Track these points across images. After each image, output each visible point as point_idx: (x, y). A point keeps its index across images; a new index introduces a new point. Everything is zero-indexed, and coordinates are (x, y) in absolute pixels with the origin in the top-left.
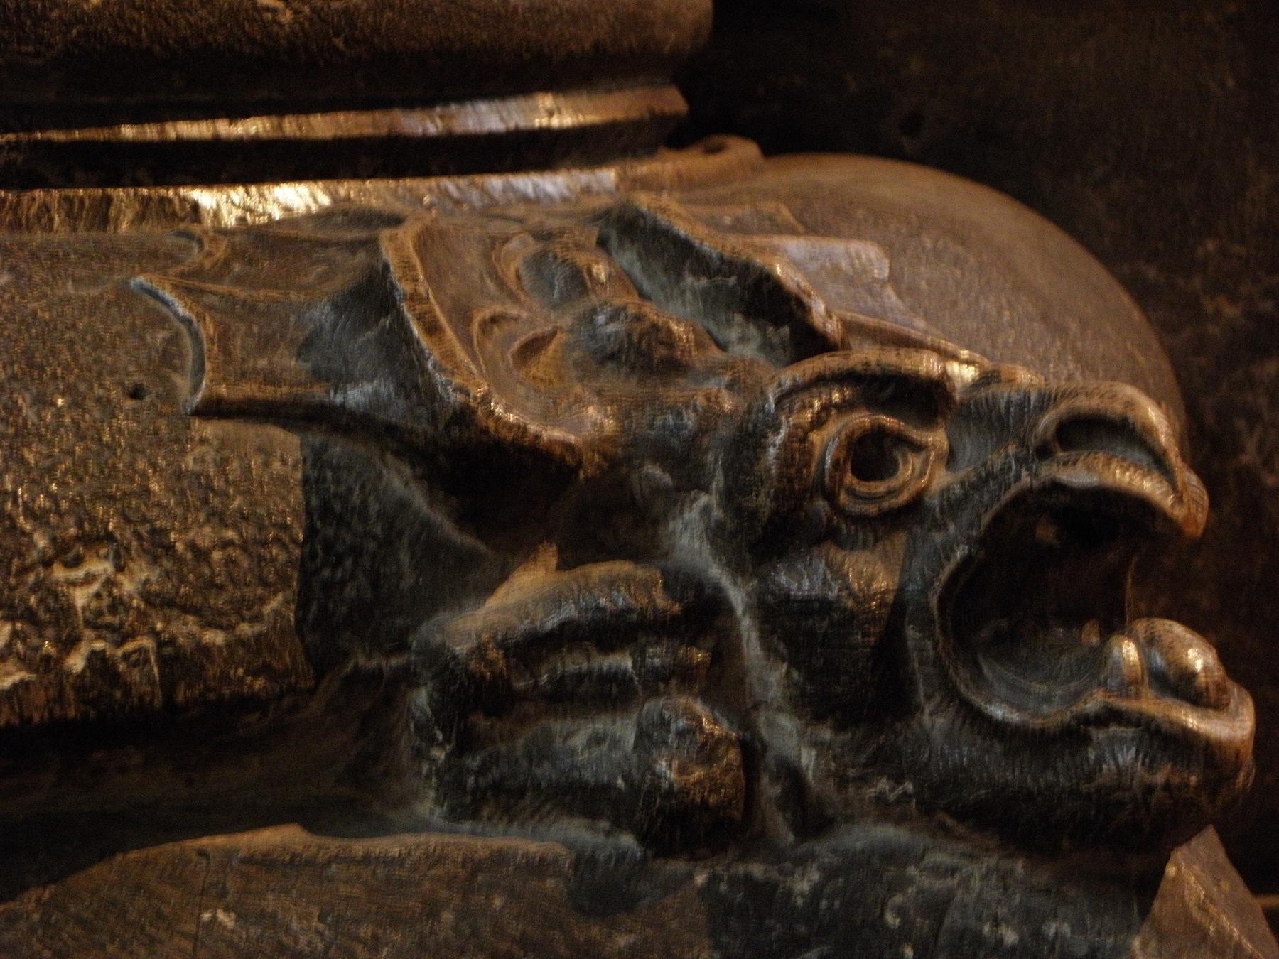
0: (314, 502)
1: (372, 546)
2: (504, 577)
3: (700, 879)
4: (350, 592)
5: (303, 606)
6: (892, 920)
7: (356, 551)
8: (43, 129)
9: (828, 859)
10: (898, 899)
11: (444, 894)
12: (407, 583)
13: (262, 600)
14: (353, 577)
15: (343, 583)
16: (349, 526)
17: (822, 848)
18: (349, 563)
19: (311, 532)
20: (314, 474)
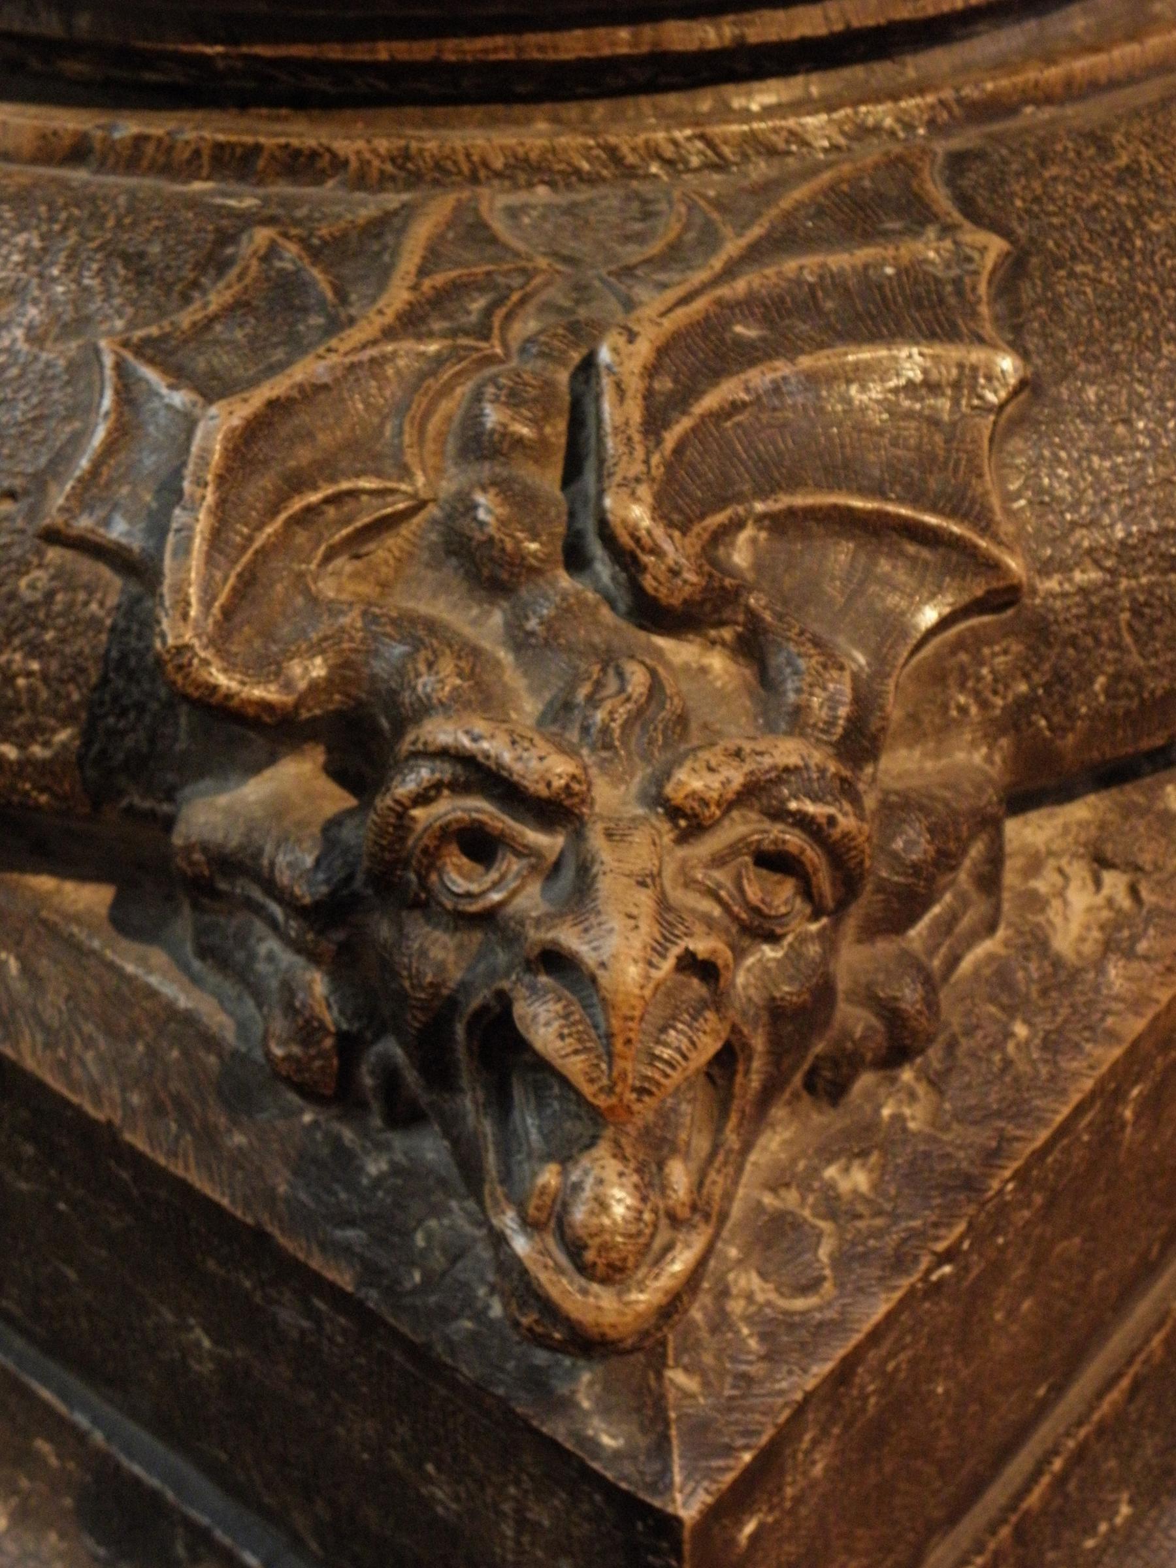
0: (114, 654)
1: (154, 706)
2: (272, 759)
3: (307, 1118)
4: (129, 742)
5: (87, 743)
6: (420, 1240)
7: (141, 708)
8: (251, 42)
9: (399, 1157)
10: (433, 1223)
11: (145, 1026)
12: (180, 746)
13: (54, 731)
14: (133, 729)
15: (123, 734)
16: (138, 682)
17: (398, 1141)
18: (132, 715)
19: (105, 681)
20: (122, 624)
